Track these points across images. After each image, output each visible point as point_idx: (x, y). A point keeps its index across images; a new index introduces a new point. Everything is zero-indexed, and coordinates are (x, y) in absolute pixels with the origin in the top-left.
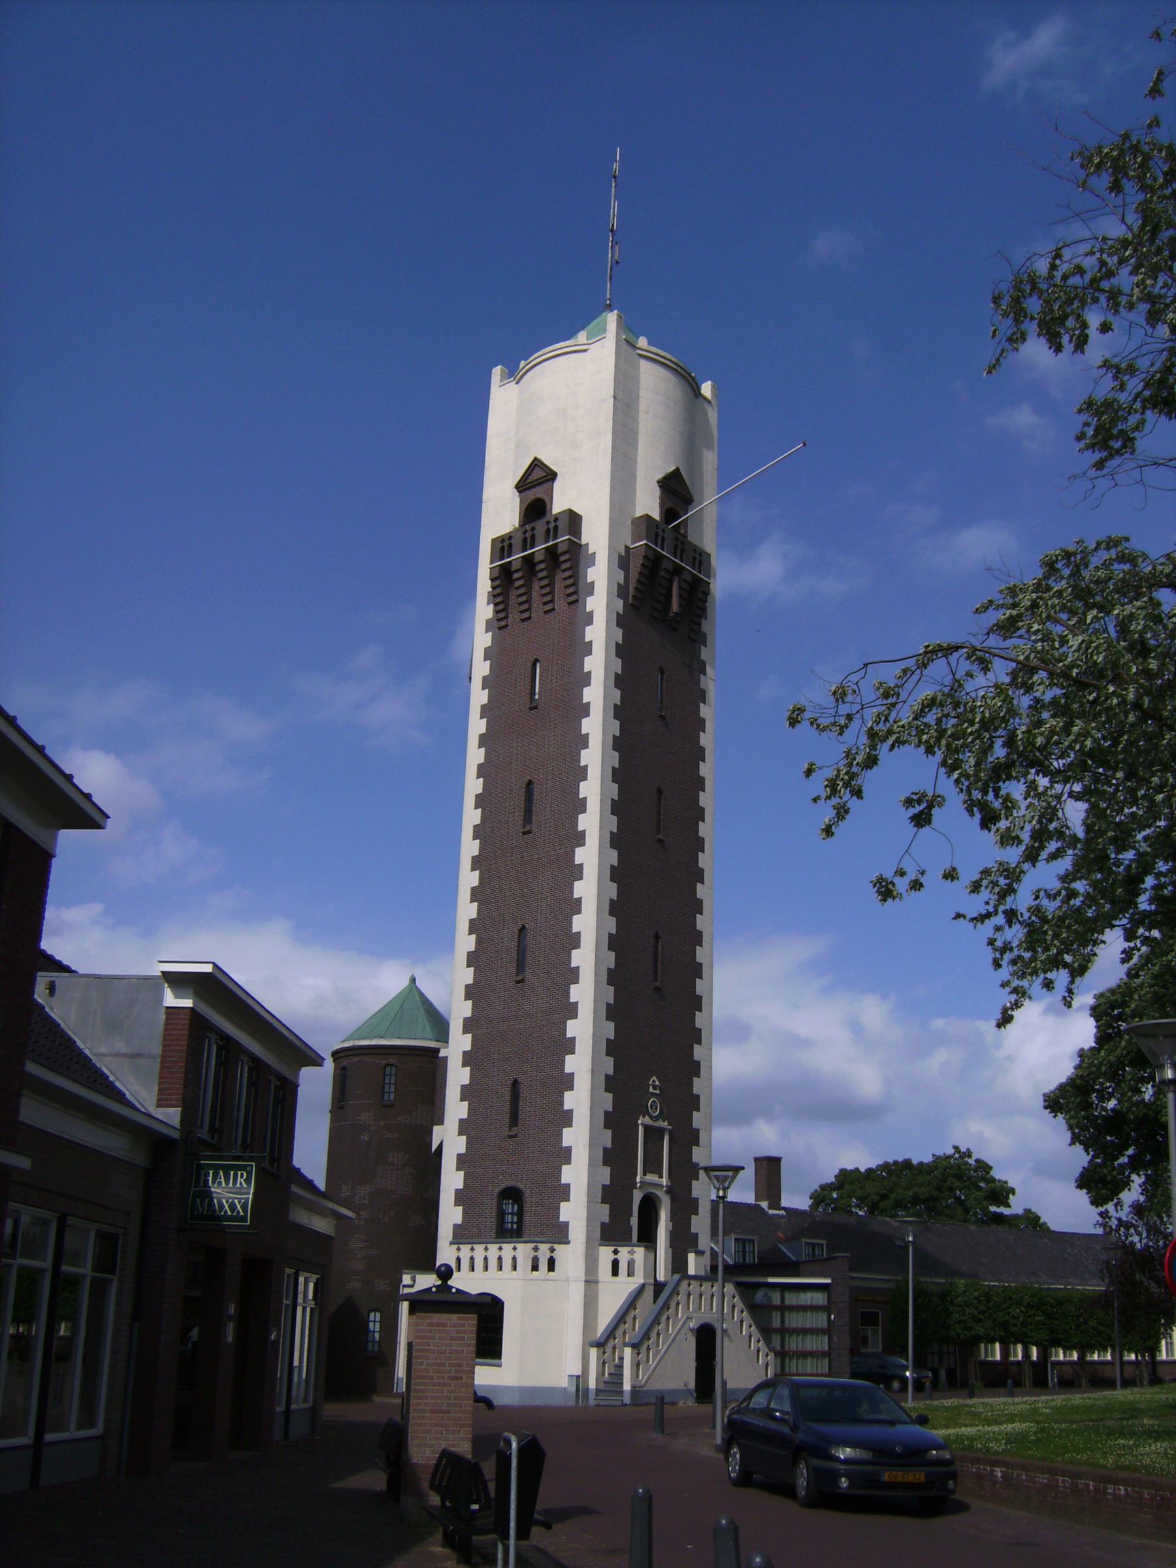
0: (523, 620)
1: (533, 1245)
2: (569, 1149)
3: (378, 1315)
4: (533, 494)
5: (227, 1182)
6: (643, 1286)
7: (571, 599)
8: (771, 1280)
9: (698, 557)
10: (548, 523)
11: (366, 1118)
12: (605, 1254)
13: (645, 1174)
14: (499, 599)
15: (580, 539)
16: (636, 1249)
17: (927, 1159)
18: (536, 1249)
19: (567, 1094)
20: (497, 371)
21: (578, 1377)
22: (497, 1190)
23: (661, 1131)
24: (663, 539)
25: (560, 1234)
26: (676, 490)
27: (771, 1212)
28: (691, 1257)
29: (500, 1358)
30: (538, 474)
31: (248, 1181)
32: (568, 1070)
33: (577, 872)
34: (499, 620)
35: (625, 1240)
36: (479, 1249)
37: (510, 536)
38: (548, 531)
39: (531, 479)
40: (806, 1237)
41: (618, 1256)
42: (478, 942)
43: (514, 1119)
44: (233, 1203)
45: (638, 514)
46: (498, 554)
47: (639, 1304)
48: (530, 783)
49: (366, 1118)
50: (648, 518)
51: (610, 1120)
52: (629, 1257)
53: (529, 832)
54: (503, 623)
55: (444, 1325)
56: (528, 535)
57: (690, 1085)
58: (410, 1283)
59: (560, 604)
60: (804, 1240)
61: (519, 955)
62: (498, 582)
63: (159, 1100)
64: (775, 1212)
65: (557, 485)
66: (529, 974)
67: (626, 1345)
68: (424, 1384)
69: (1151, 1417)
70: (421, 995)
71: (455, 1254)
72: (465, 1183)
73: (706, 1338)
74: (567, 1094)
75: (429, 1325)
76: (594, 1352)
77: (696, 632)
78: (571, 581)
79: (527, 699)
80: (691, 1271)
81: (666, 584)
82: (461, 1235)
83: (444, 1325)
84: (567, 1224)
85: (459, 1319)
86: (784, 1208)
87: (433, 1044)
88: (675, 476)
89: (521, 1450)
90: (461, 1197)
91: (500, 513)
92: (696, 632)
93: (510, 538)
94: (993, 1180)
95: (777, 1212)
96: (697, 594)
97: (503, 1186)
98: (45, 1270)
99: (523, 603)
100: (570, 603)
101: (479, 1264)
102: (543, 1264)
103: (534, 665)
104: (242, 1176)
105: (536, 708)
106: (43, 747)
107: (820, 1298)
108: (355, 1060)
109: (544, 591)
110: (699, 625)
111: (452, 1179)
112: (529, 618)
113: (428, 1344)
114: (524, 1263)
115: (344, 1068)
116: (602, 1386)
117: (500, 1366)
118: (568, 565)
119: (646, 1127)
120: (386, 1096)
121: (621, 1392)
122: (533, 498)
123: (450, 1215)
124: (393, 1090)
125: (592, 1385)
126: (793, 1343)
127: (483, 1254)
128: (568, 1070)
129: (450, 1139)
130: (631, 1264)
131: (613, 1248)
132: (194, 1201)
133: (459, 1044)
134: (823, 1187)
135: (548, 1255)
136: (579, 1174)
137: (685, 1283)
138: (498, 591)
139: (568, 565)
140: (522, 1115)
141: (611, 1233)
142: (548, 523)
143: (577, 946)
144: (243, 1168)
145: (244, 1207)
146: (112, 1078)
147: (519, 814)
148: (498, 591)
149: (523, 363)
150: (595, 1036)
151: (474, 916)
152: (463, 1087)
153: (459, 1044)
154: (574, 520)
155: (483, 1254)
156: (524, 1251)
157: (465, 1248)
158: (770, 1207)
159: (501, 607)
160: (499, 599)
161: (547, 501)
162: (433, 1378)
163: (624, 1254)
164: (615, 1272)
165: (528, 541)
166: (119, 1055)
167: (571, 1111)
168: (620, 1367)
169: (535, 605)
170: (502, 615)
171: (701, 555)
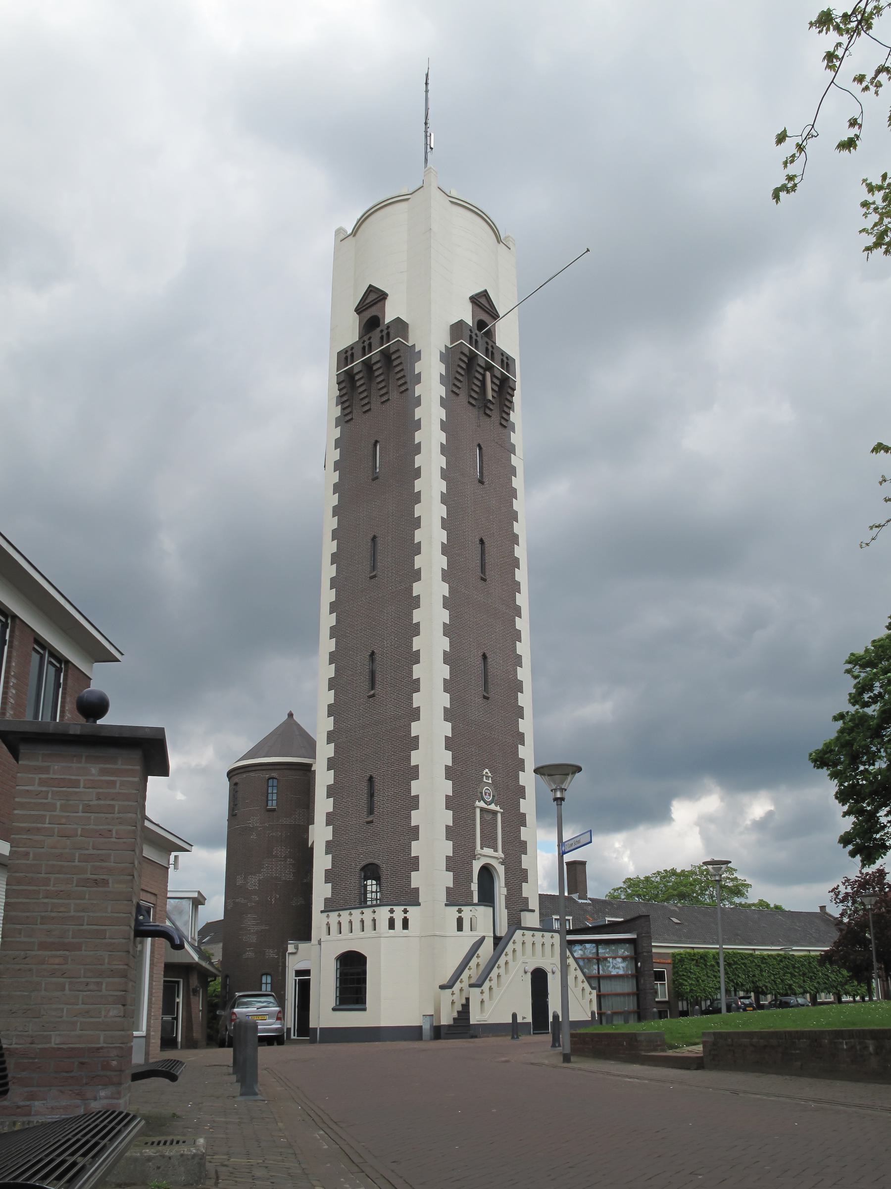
0: (365, 412)
1: (389, 908)
2: (417, 828)
6: (483, 938)
7: (403, 388)
9: (505, 359)
10: (382, 331)
15: (407, 339)
22: (359, 867)
23: (495, 813)
25: (412, 898)
27: (580, 901)
29: (365, 1003)
30: (372, 297)
34: (346, 415)
36: (345, 914)
37: (352, 347)
38: (382, 338)
41: (462, 915)
42: (337, 670)
46: (343, 362)
48: (374, 538)
52: (458, 915)
53: (375, 576)
54: (349, 417)
55: (75, 784)
56: (366, 344)
57: (517, 778)
58: (294, 951)
59: (394, 395)
61: (372, 675)
65: (388, 303)
71: (325, 921)
72: (333, 864)
73: (539, 978)
75: (42, 782)
77: (507, 420)
81: (480, 377)
82: (330, 906)
83: (76, 784)
85: (103, 772)
86: (590, 899)
92: (507, 420)
93: (352, 348)
97: (363, 863)
99: (366, 404)
100: (402, 393)
102: (398, 924)
105: (377, 478)
108: (244, 776)
110: (509, 414)
111: (322, 862)
112: (370, 410)
114: (383, 924)
115: (236, 784)
117: (365, 1010)
119: (482, 810)
120: (270, 803)
122: (369, 316)
123: (321, 890)
124: (275, 798)
126: (606, 987)
129: (320, 834)
133: (325, 751)
135: (403, 915)
136: (432, 848)
137: (519, 933)
138: (344, 391)
148: (344, 391)
152: (329, 787)
156: (383, 913)
157: (334, 915)
158: (580, 898)
161: (380, 317)
163: (467, 912)
164: (460, 928)
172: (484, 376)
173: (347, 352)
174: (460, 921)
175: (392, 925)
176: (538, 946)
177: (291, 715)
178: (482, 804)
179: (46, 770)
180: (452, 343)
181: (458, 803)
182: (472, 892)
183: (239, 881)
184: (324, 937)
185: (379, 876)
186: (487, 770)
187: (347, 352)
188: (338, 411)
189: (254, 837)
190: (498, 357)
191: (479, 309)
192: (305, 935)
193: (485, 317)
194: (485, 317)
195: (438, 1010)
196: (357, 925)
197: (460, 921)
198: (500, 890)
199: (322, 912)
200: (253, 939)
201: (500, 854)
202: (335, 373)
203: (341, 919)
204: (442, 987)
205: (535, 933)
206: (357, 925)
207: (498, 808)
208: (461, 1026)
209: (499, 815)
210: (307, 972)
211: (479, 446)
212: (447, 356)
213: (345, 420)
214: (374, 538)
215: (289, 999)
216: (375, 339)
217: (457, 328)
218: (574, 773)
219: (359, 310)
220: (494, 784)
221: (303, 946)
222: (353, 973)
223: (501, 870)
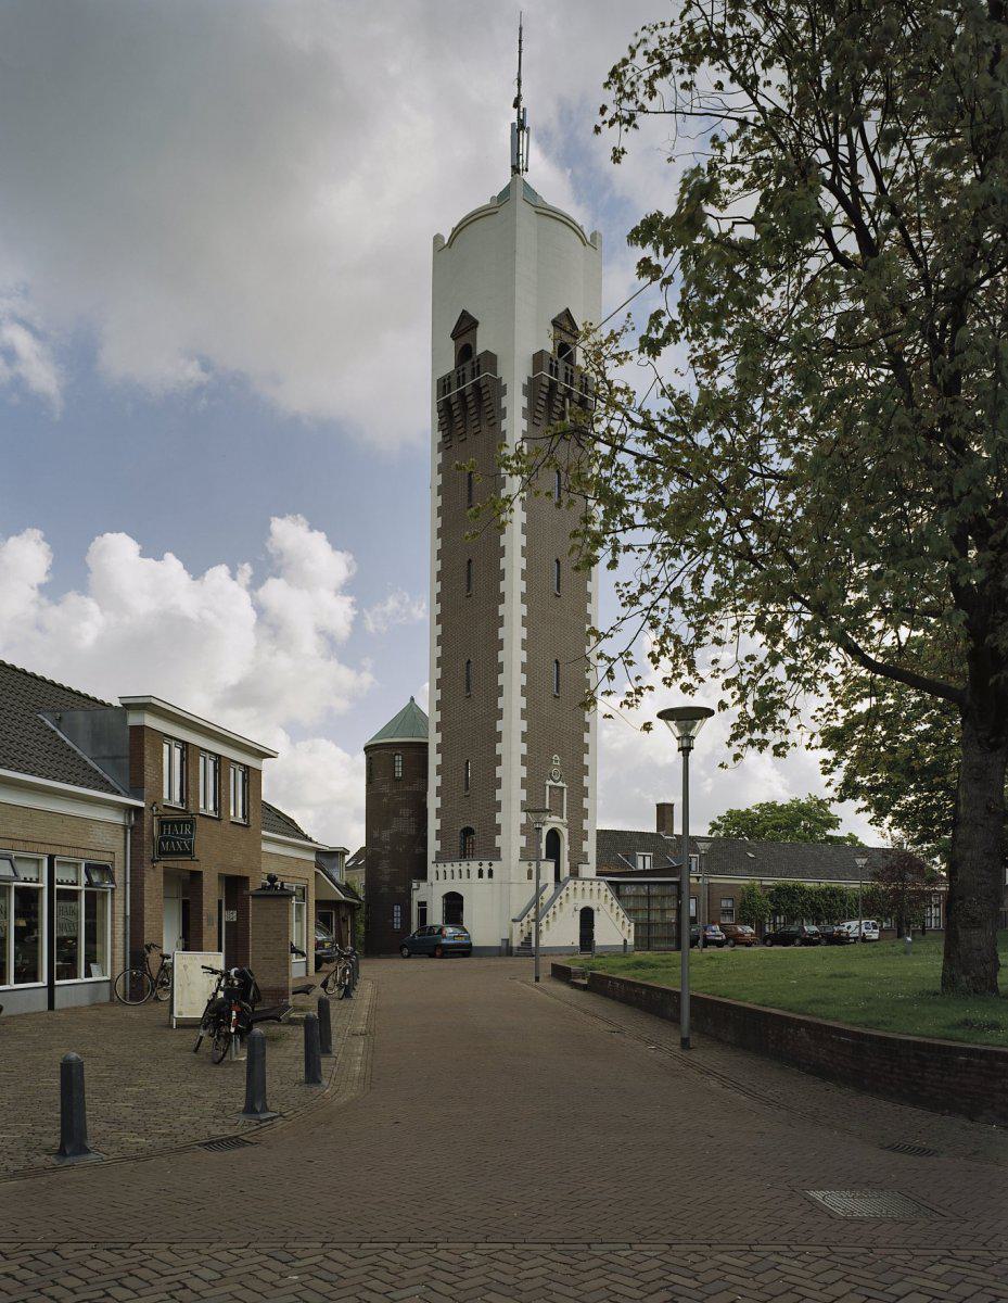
4: (464, 340)
7: (492, 422)
10: (473, 363)
11: (385, 789)
18: (530, 865)
23: (562, 788)
25: (495, 854)
30: (466, 324)
37: (449, 376)
49: (385, 789)
52: (467, 867)
56: (461, 374)
59: (484, 427)
65: (480, 331)
69: (366, 933)
73: (587, 916)
90: (439, 835)
94: (829, 814)
98: (42, 888)
102: (486, 874)
106: (454, 230)
109: (490, 408)
111: (434, 824)
114: (474, 873)
123: (434, 846)
127: (467, 867)
129: (433, 802)
133: (434, 739)
136: (512, 818)
138: (444, 420)
144: (188, 822)
147: (464, 583)
148: (444, 420)
156: (474, 866)
164: (481, 875)
165: (461, 380)
166: (104, 758)
168: (530, 934)
173: (445, 380)
175: (481, 874)
176: (595, 892)
177: (412, 699)
178: (551, 783)
181: (531, 784)
183: (376, 835)
184: (435, 881)
185: (473, 842)
187: (445, 380)
188: (439, 437)
189: (385, 800)
192: (423, 876)
193: (567, 339)
195: (511, 936)
196: (457, 874)
198: (565, 848)
200: (387, 878)
201: (565, 820)
202: (436, 401)
204: (514, 921)
206: (457, 874)
208: (528, 949)
210: (425, 903)
212: (531, 389)
213: (445, 447)
214: (470, 561)
215: (120, 921)
216: (468, 372)
217: (538, 358)
218: (706, 717)
219: (455, 336)
220: (562, 767)
221: (422, 884)
222: (454, 904)
223: (565, 833)
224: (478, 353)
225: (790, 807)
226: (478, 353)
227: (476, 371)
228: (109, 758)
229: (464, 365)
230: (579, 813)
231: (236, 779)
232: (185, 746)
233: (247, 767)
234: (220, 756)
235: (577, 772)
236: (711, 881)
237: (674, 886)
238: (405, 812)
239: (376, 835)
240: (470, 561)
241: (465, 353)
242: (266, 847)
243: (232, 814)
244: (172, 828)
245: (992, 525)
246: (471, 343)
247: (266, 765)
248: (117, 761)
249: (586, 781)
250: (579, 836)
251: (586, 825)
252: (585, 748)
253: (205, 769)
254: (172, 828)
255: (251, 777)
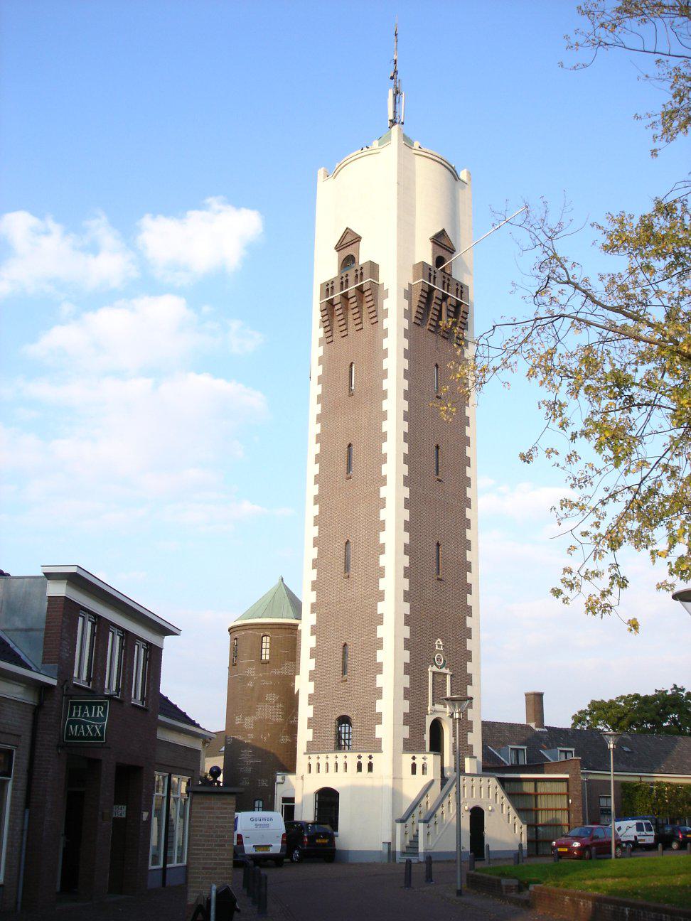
1: (357, 754)
3: (261, 803)
4: (347, 252)
5: (91, 714)
7: (374, 320)
8: (522, 776)
9: (460, 288)
10: (357, 270)
11: (251, 672)
12: (407, 759)
13: (433, 705)
14: (327, 323)
15: (378, 280)
16: (427, 756)
17: (651, 693)
18: (360, 757)
19: (379, 652)
20: (321, 172)
21: (389, 844)
24: (435, 278)
25: (376, 746)
26: (442, 242)
27: (537, 730)
28: (467, 760)
30: (348, 239)
31: (104, 713)
32: (379, 636)
33: (382, 503)
35: (421, 749)
36: (323, 756)
38: (357, 276)
39: (345, 242)
40: (560, 746)
41: (427, 761)
42: (320, 553)
43: (344, 671)
44: (94, 728)
45: (418, 261)
47: (430, 793)
49: (251, 672)
50: (423, 263)
51: (408, 669)
52: (412, 761)
54: (330, 339)
56: (344, 280)
58: (281, 781)
60: (510, 746)
62: (325, 312)
63: (44, 659)
64: (540, 730)
65: (363, 245)
66: (352, 572)
67: (420, 821)
68: (198, 850)
70: (285, 586)
74: (379, 652)
76: (399, 826)
78: (373, 309)
79: (347, 389)
80: (467, 771)
81: (438, 308)
82: (312, 748)
83: (213, 808)
84: (380, 740)
86: (546, 727)
87: (294, 621)
88: (442, 234)
89: (218, 895)
91: (327, 267)
95: (542, 730)
96: (460, 312)
101: (332, 767)
102: (365, 767)
103: (351, 366)
104: (100, 709)
107: (562, 788)
111: (305, 711)
113: (201, 822)
116: (405, 850)
118: (370, 298)
119: (434, 673)
121: (417, 854)
122: (347, 255)
123: (304, 735)
124: (268, 646)
125: (398, 849)
127: (368, 760)
128: (379, 636)
129: (304, 686)
130: (424, 768)
131: (412, 755)
132: (68, 728)
133: (307, 621)
134: (581, 712)
135: (368, 760)
138: (326, 318)
139: (370, 298)
140: (349, 667)
141: (411, 745)
142: (357, 270)
143: (383, 553)
144: (101, 704)
145: (102, 730)
146: (12, 645)
148: (326, 318)
149: (337, 165)
150: (396, 612)
151: (316, 535)
153: (307, 621)
154: (373, 268)
155: (335, 760)
156: (352, 758)
157: (314, 757)
159: (328, 329)
160: (327, 323)
162: (204, 845)
164: (414, 772)
166: (17, 630)
167: (381, 664)
168: (416, 836)
169: (350, 327)
170: (329, 334)
171: (461, 287)
172: (441, 306)
174: (414, 766)
178: (435, 669)
179: (203, 803)
180: (414, 281)
181: (414, 669)
182: (425, 742)
186: (439, 640)
190: (453, 287)
191: (438, 247)
192: (291, 769)
193: (442, 253)
194: (442, 253)
197: (414, 766)
199: (304, 754)
200: (249, 770)
203: (320, 761)
205: (474, 778)
207: (447, 671)
209: (448, 678)
211: (437, 365)
214: (350, 445)
221: (291, 777)
224: (360, 263)
225: (655, 698)
226: (360, 263)
227: (359, 276)
228: (21, 630)
229: (348, 272)
230: (462, 700)
231: (139, 654)
232: (99, 621)
233: (148, 644)
234: (127, 632)
235: (460, 658)
236: (591, 777)
237: (565, 784)
238: (271, 697)
239: (238, 721)
240: (350, 445)
241: (348, 261)
242: (163, 735)
243: (133, 696)
244: (83, 710)
245: (607, 449)
246: (354, 254)
247: (168, 643)
248: (31, 633)
249: (470, 668)
250: (464, 726)
251: (471, 715)
252: (468, 633)
253: (114, 643)
254: (83, 710)
255: (154, 655)
